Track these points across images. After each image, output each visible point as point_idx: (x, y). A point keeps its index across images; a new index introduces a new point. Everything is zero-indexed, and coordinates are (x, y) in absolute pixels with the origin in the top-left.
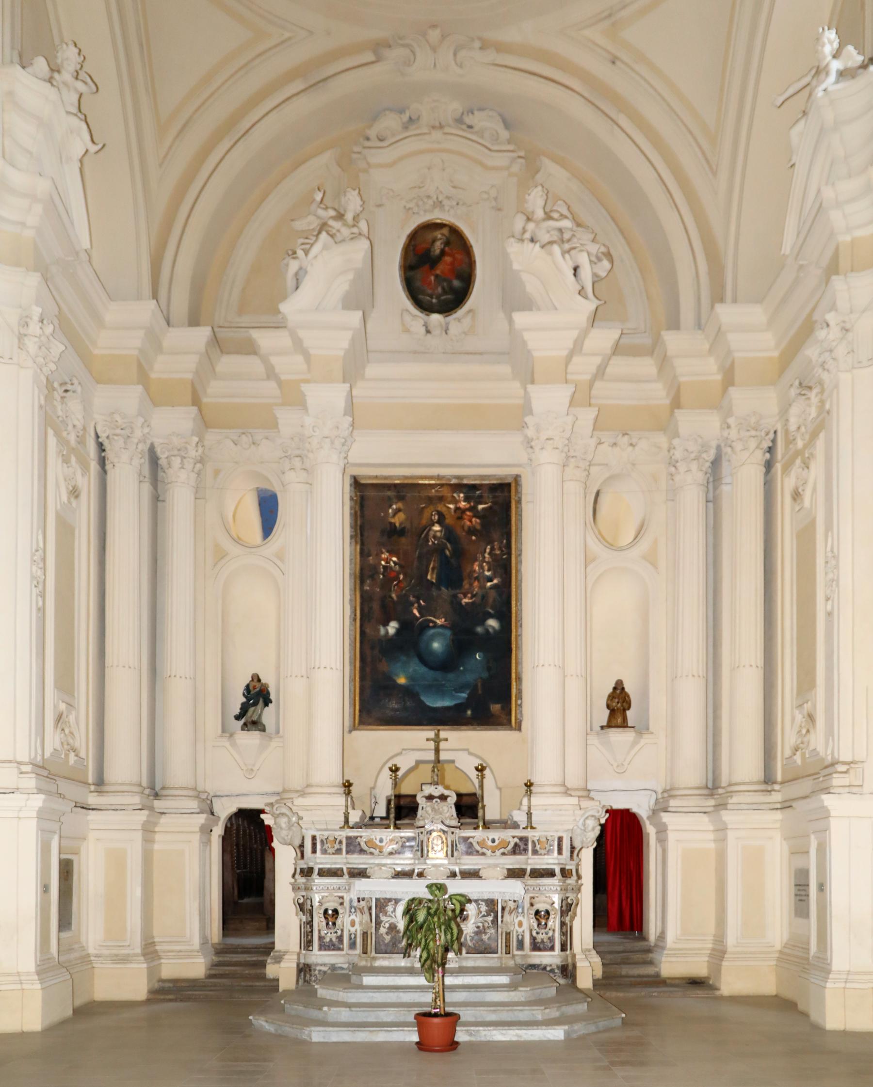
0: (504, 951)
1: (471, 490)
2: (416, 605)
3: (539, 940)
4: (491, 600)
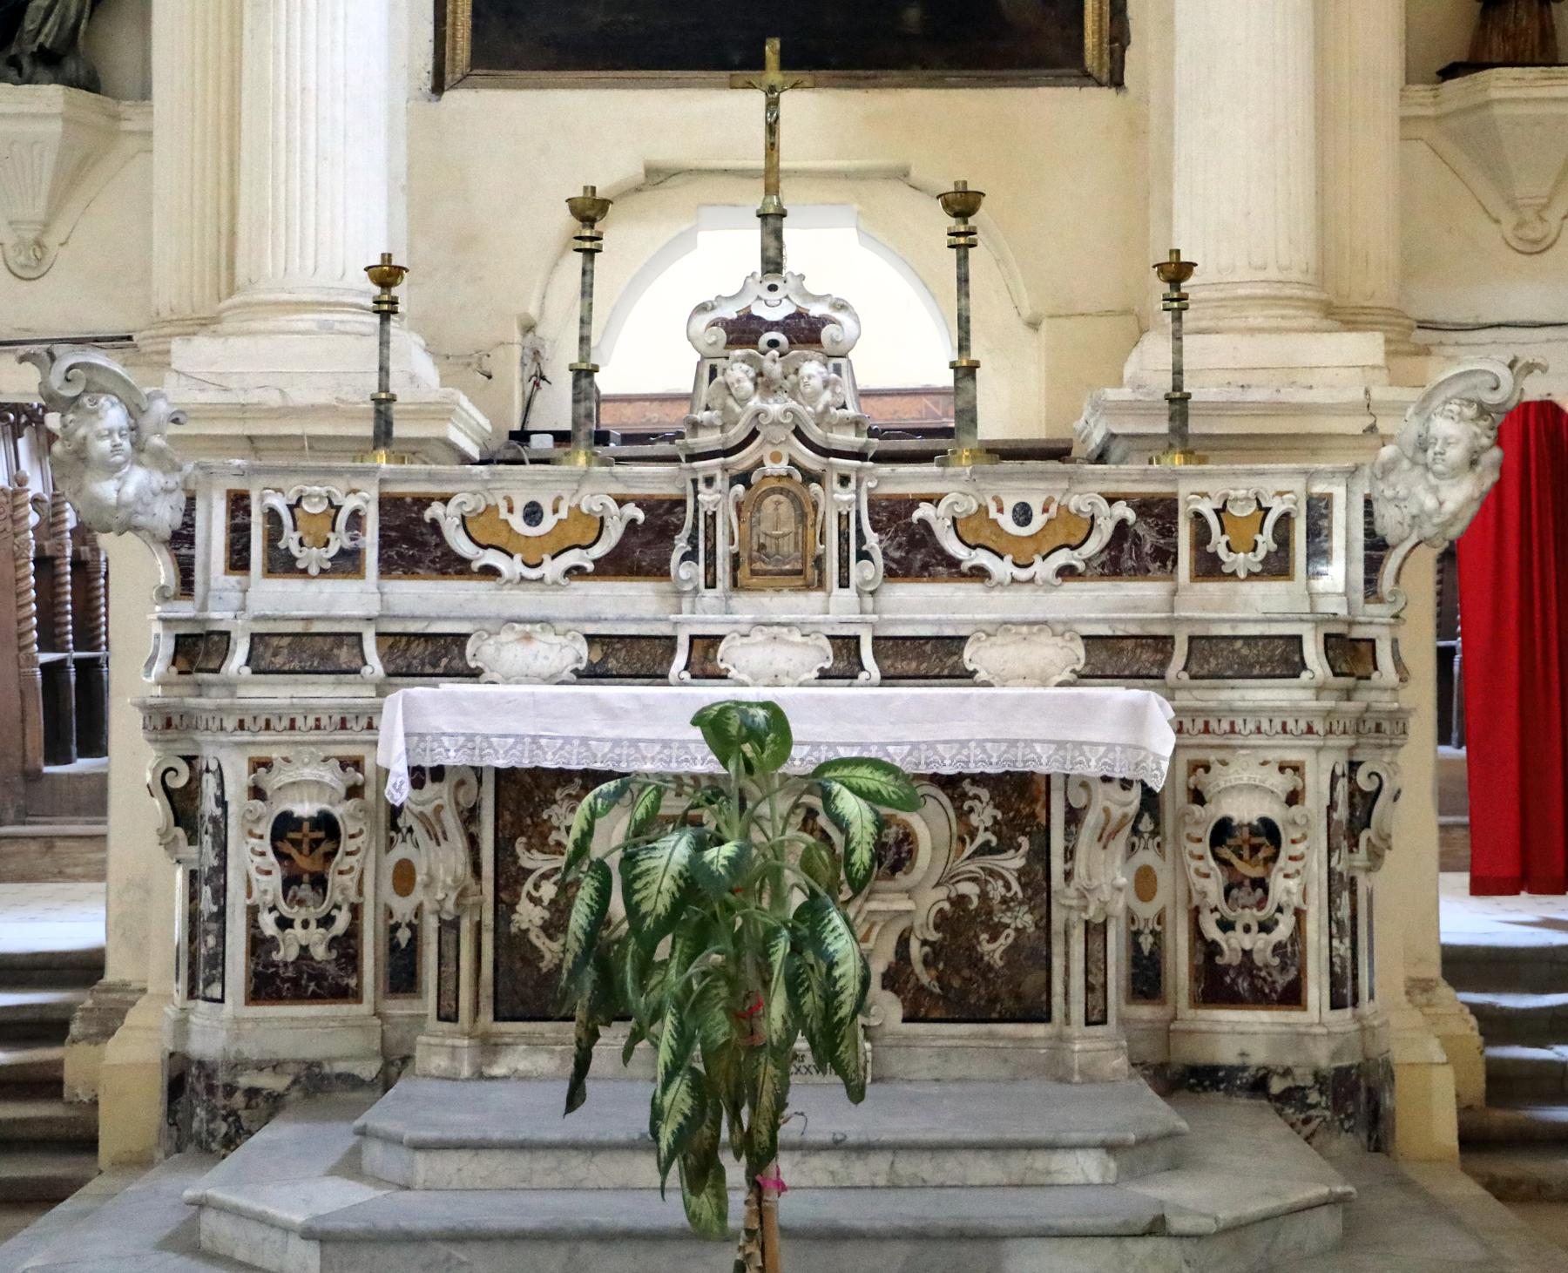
0: (1078, 1012)
3: (1230, 957)
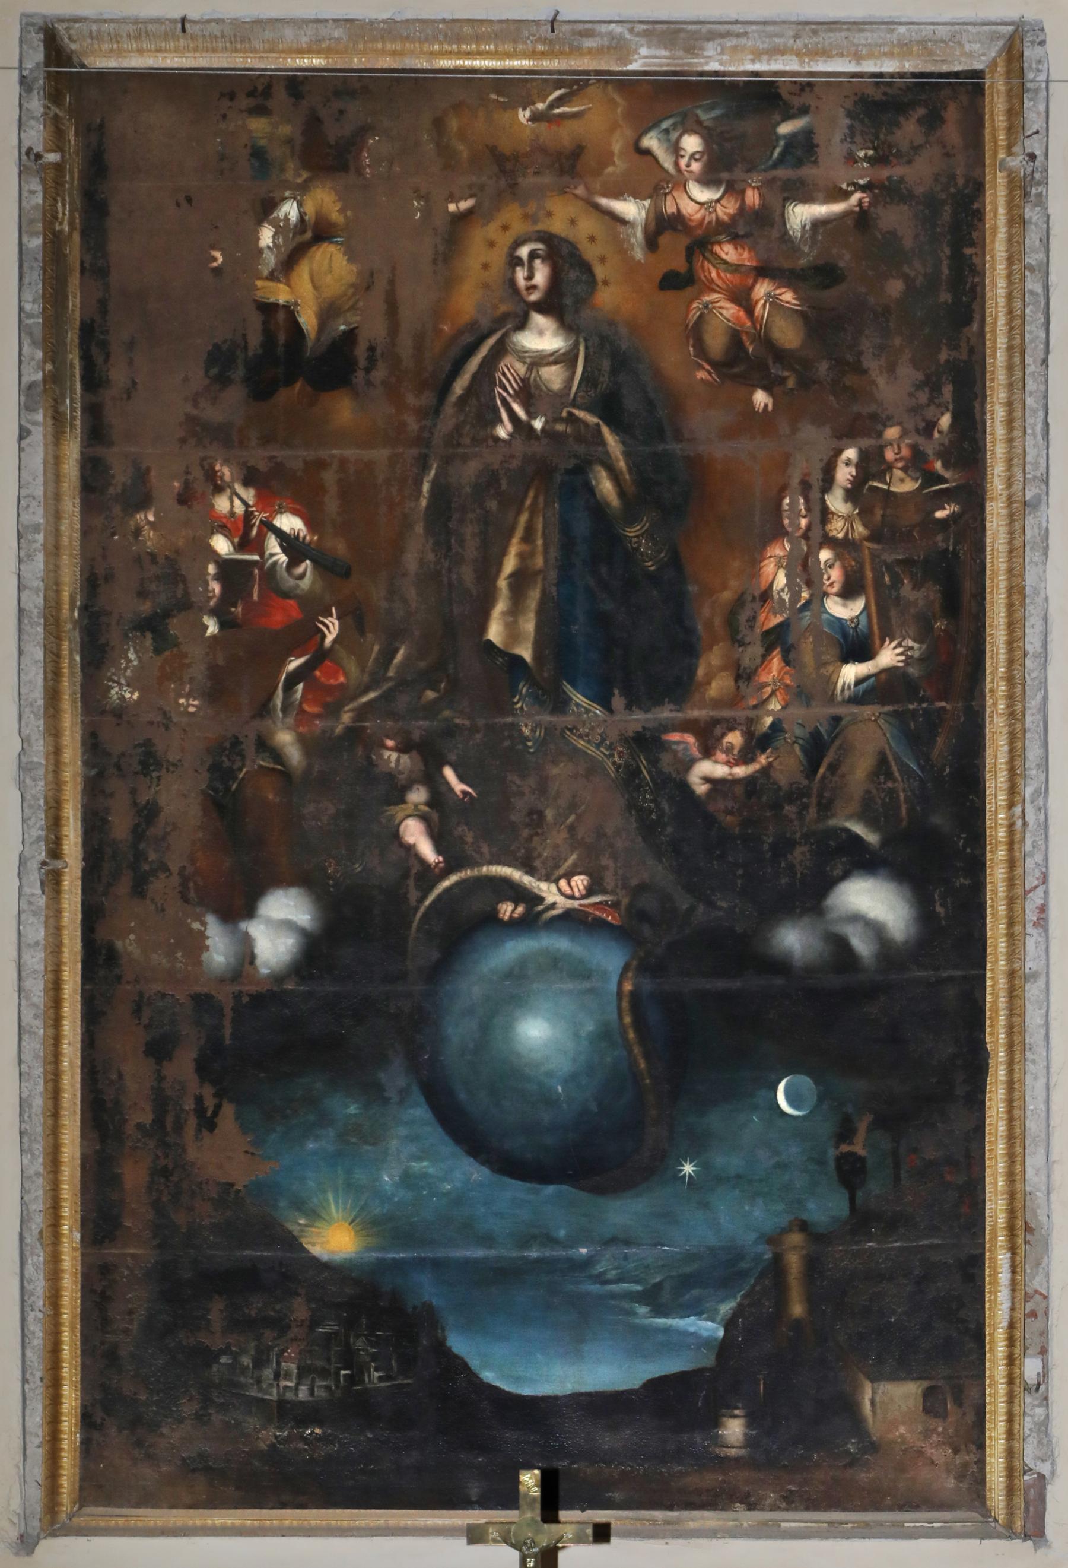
2: (418, 796)
4: (859, 771)
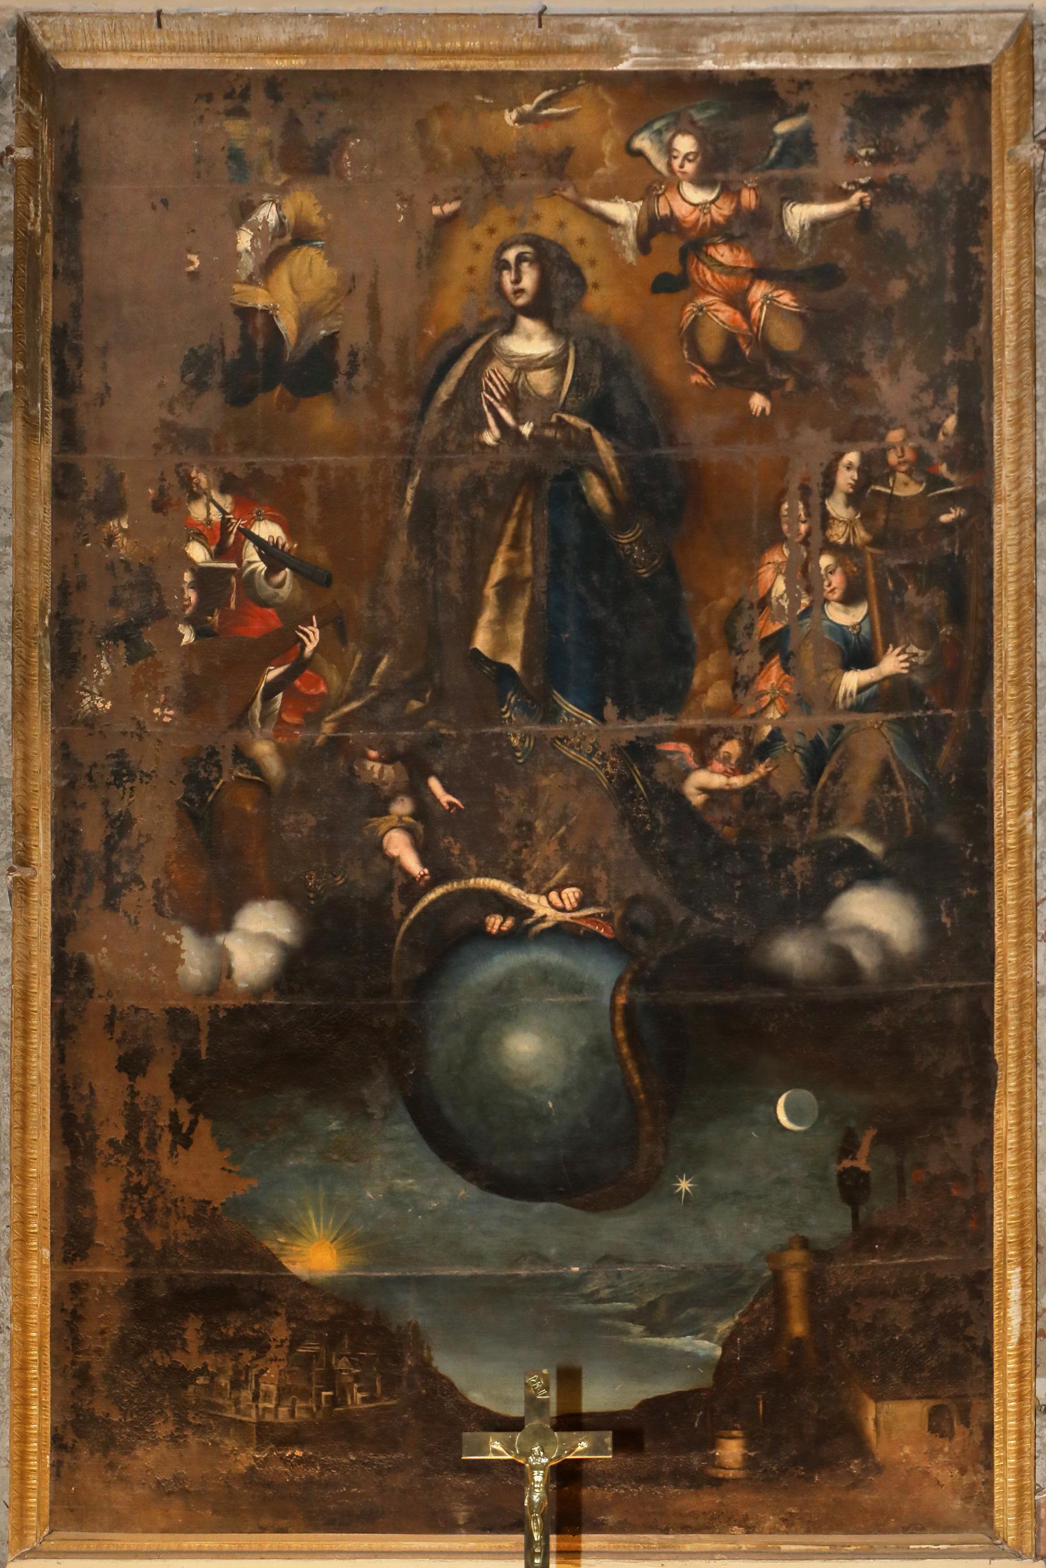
1: (742, 115)
2: (402, 807)
